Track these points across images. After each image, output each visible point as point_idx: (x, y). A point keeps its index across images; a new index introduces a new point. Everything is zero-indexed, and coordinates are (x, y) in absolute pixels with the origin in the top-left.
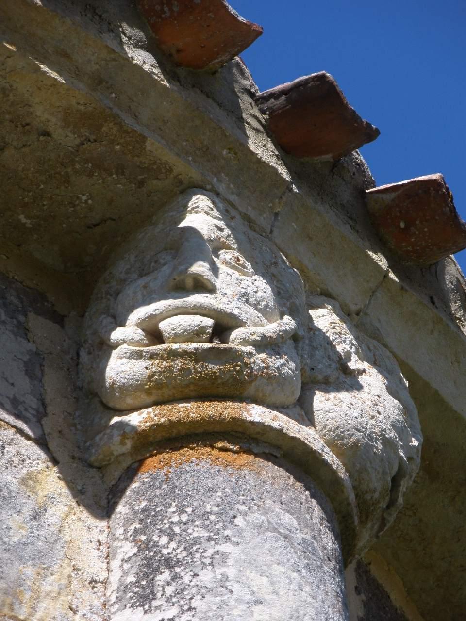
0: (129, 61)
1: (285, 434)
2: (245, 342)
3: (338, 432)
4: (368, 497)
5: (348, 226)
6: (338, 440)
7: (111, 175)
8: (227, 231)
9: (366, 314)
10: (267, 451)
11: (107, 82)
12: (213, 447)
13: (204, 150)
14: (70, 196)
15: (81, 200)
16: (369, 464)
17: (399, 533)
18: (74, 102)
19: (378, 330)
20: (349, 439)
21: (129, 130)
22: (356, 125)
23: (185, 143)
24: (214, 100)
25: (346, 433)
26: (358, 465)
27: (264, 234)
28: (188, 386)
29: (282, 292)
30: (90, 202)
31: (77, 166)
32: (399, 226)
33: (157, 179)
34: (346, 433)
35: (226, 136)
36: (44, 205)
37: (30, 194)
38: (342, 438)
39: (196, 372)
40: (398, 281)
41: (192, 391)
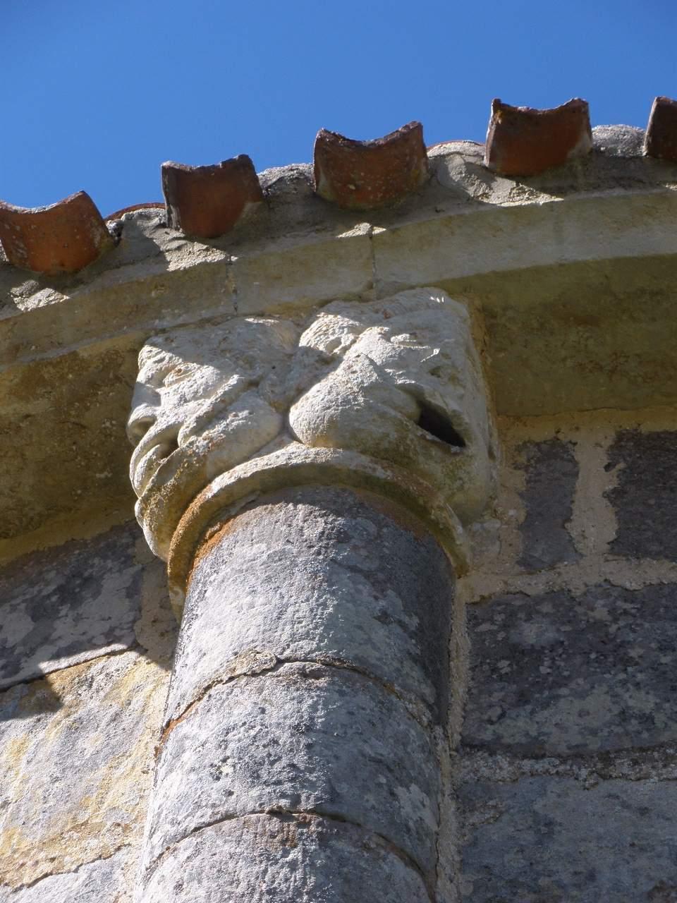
0: (37, 310)
1: (245, 478)
2: (186, 437)
3: (312, 426)
4: (385, 444)
6: (316, 433)
7: (98, 394)
8: (167, 355)
9: (378, 281)
10: (243, 504)
11: (22, 344)
12: (206, 541)
13: (135, 309)
14: (99, 433)
15: (108, 427)
17: (640, 379)
18: (7, 383)
19: (396, 282)
20: (323, 423)
21: (59, 360)
22: (213, 174)
23: (115, 322)
24: (125, 264)
25: (318, 421)
27: (229, 318)
28: (169, 512)
29: (238, 356)
30: (114, 422)
31: (73, 413)
32: (352, 190)
33: (120, 365)
34: (318, 421)
35: (143, 283)
36: (96, 455)
37: (79, 458)
38: (317, 428)
39: (164, 496)
40: (384, 230)
41: (176, 512)
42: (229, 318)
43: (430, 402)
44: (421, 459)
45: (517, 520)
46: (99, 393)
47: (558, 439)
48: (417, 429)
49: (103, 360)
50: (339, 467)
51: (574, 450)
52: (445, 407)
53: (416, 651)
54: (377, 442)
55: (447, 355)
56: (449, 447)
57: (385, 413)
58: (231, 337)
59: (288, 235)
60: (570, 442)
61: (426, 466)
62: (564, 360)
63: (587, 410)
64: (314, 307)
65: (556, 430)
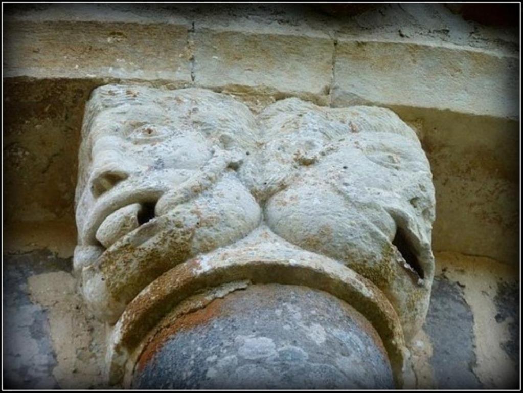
4: (370, 264)
5: (276, 23)
10: (232, 289)
16: (350, 238)
19: (355, 95)
23: (66, 57)
26: (339, 245)
27: (186, 85)
30: (27, 153)
42: (186, 85)
43: (410, 231)
44: (395, 284)
45: (425, 353)
46: (26, 122)
47: (445, 277)
48: (399, 256)
49: (47, 92)
50: (332, 277)
51: (463, 293)
52: (420, 239)
53: (56, 371)
54: (365, 259)
55: (424, 187)
56: (418, 278)
57: (376, 233)
58: (200, 109)
59: (250, 17)
60: (458, 283)
61: (397, 293)
62: (472, 205)
63: (470, 255)
64: (272, 97)
65: (443, 268)
